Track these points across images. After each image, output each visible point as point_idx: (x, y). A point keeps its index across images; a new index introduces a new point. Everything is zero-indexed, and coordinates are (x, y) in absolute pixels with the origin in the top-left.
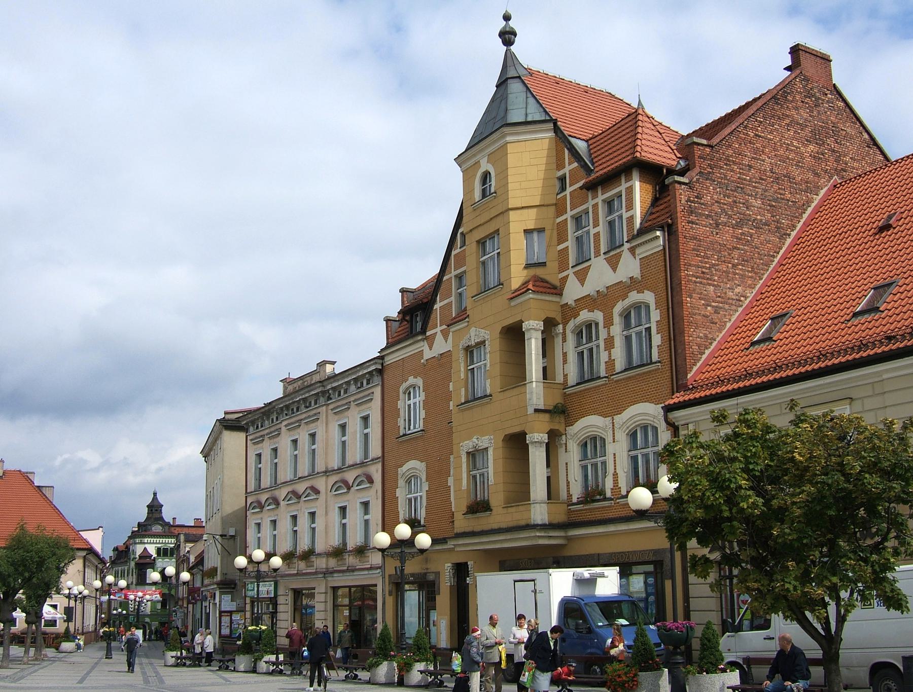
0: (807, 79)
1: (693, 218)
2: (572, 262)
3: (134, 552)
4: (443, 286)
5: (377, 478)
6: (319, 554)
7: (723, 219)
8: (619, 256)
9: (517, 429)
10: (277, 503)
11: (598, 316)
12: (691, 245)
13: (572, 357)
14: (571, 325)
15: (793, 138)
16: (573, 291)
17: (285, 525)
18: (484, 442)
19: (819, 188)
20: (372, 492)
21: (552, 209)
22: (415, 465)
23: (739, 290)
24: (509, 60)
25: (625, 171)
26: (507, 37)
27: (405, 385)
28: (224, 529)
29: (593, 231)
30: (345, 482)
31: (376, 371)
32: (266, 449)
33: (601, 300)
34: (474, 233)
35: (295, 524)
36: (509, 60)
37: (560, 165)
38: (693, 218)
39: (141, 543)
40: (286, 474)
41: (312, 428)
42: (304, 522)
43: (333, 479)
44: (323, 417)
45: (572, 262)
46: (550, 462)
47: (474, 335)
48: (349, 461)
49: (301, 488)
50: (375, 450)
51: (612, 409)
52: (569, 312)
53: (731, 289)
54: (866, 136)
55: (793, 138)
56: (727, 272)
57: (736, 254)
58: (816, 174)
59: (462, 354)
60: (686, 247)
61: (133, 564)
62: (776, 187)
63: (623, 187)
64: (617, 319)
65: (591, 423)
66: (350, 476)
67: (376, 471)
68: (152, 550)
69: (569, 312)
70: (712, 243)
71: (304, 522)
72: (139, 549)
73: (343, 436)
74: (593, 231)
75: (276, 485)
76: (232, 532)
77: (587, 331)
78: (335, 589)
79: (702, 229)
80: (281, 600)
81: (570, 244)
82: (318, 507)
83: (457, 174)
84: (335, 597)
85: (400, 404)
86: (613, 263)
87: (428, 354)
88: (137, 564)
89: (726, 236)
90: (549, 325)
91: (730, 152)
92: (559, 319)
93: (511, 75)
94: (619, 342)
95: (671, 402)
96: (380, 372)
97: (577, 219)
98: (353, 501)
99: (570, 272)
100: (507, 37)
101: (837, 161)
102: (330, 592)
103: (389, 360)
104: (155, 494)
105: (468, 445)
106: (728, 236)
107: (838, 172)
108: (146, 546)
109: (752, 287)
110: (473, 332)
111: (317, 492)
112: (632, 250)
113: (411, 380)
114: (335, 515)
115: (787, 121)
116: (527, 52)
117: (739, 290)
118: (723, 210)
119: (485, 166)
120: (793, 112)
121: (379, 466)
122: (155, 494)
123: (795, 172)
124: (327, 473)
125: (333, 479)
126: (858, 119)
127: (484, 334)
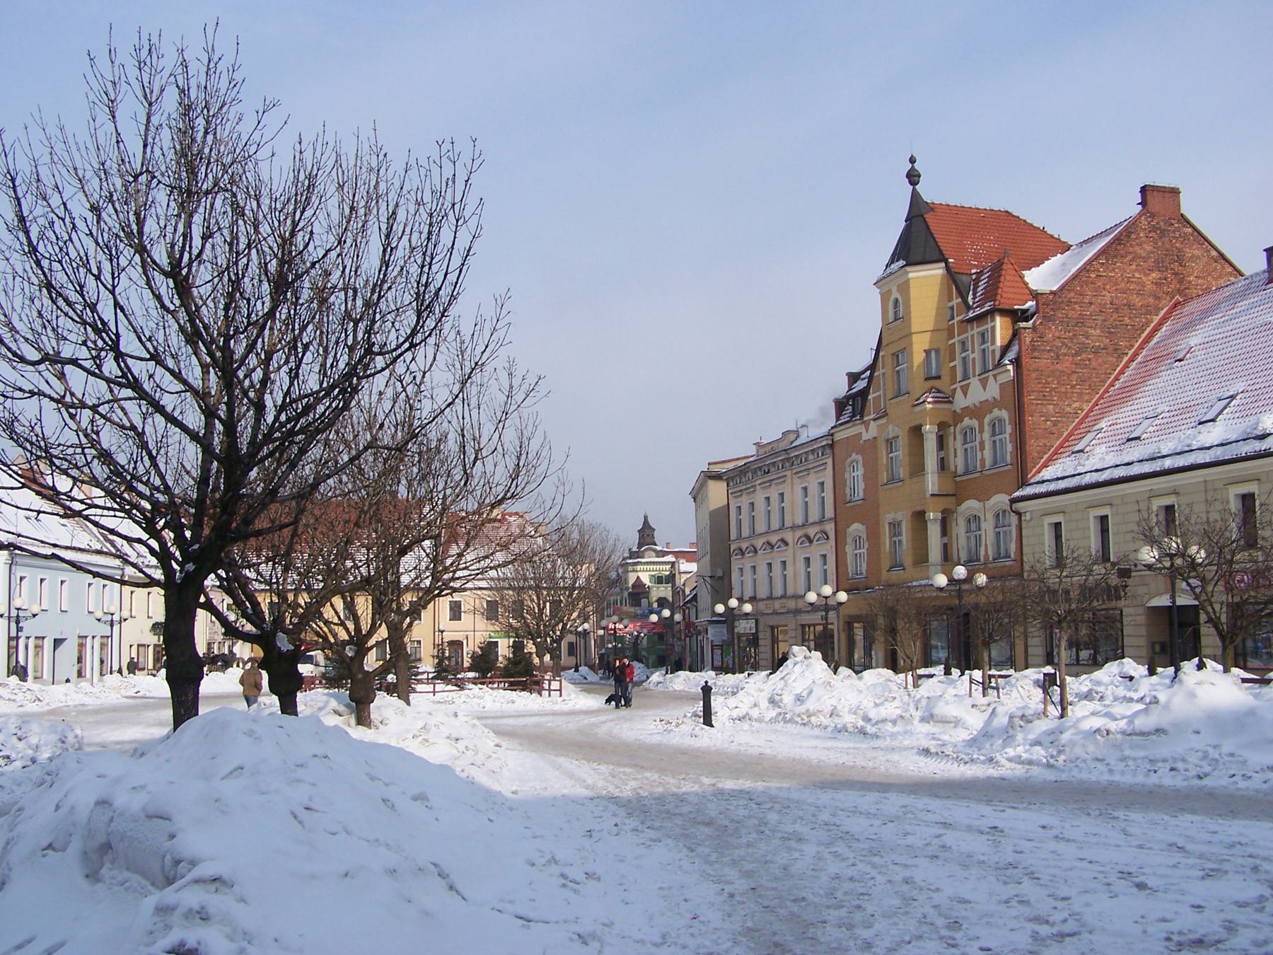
0: (1153, 216)
1: (1036, 354)
2: (959, 378)
3: (626, 580)
4: (874, 381)
5: (832, 535)
6: (762, 600)
7: (1063, 351)
8: (987, 378)
9: (919, 508)
10: (756, 551)
11: (975, 423)
12: (1034, 375)
13: (960, 453)
14: (959, 428)
15: (1136, 270)
16: (960, 402)
17: (762, 570)
18: (899, 516)
19: (1158, 309)
20: (828, 546)
21: (945, 333)
22: (857, 528)
23: (1076, 405)
24: (915, 196)
25: (991, 313)
26: (913, 177)
27: (849, 460)
28: (712, 570)
29: (972, 356)
30: (808, 537)
31: (830, 445)
32: (744, 502)
33: (977, 412)
34: (891, 345)
35: (785, 569)
36: (915, 196)
37: (950, 299)
38: (1036, 354)
39: (634, 571)
40: (761, 527)
41: (781, 489)
42: (777, 568)
43: (799, 533)
44: (789, 481)
45: (959, 378)
46: (944, 532)
47: (892, 431)
48: (811, 520)
49: (774, 539)
50: (829, 513)
51: (983, 498)
52: (957, 417)
53: (1069, 405)
54: (1214, 253)
55: (1136, 270)
56: (1066, 393)
57: (1074, 377)
58: (1157, 298)
59: (884, 444)
60: (1030, 378)
61: (626, 594)
62: (1115, 315)
63: (989, 326)
64: (986, 427)
65: (971, 505)
66: (812, 531)
67: (830, 528)
68: (645, 578)
69: (957, 417)
70: (1053, 372)
71: (777, 568)
72: (632, 578)
73: (805, 496)
74: (972, 356)
75: (753, 534)
76: (720, 573)
77: (967, 435)
78: (803, 626)
79: (1044, 362)
80: (761, 635)
81: (957, 363)
82: (788, 554)
83: (876, 293)
84: (803, 633)
85: (847, 475)
86: (984, 383)
87: (865, 437)
88: (630, 594)
89: (1066, 365)
90: (942, 426)
91: (1072, 294)
92: (951, 422)
93: (918, 211)
94: (988, 445)
95: (1017, 494)
96: (831, 446)
97: (963, 343)
98: (815, 552)
99: (957, 385)
100: (913, 177)
101: (1181, 282)
102: (800, 629)
103: (838, 437)
104: (646, 518)
105: (889, 517)
106: (1067, 364)
107: (1180, 292)
108: (640, 574)
109: (1088, 401)
110: (890, 428)
111: (787, 544)
112: (995, 376)
113: (854, 456)
114: (801, 565)
115: (1129, 257)
116: (928, 192)
117: (1076, 405)
118: (1063, 343)
119: (895, 294)
120: (1137, 248)
121: (833, 525)
122: (646, 518)
123: (1136, 300)
124: (794, 528)
125: (799, 533)
126: (1206, 240)
127: (898, 431)
